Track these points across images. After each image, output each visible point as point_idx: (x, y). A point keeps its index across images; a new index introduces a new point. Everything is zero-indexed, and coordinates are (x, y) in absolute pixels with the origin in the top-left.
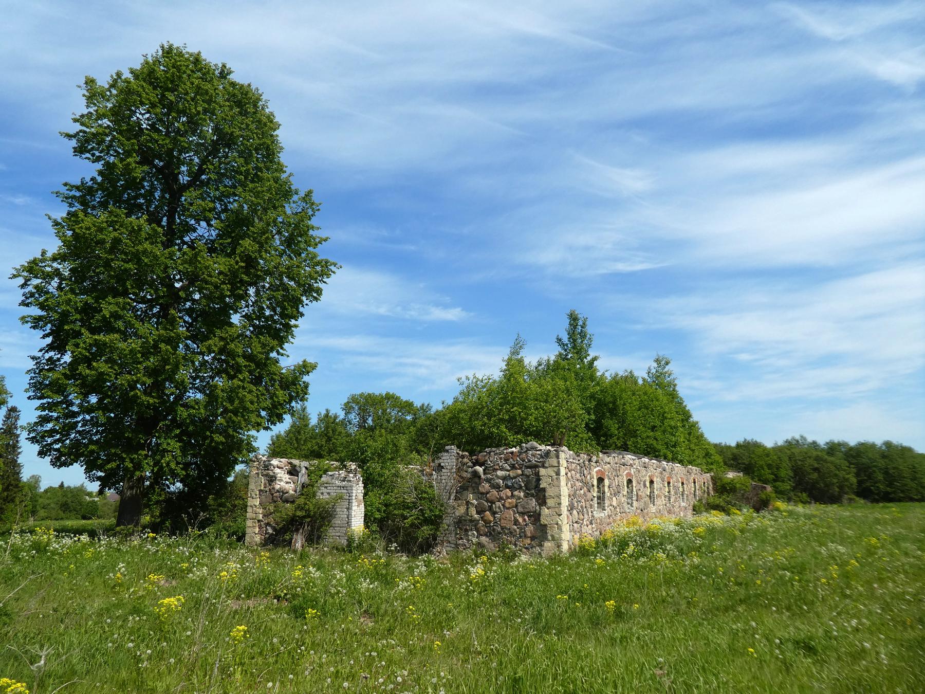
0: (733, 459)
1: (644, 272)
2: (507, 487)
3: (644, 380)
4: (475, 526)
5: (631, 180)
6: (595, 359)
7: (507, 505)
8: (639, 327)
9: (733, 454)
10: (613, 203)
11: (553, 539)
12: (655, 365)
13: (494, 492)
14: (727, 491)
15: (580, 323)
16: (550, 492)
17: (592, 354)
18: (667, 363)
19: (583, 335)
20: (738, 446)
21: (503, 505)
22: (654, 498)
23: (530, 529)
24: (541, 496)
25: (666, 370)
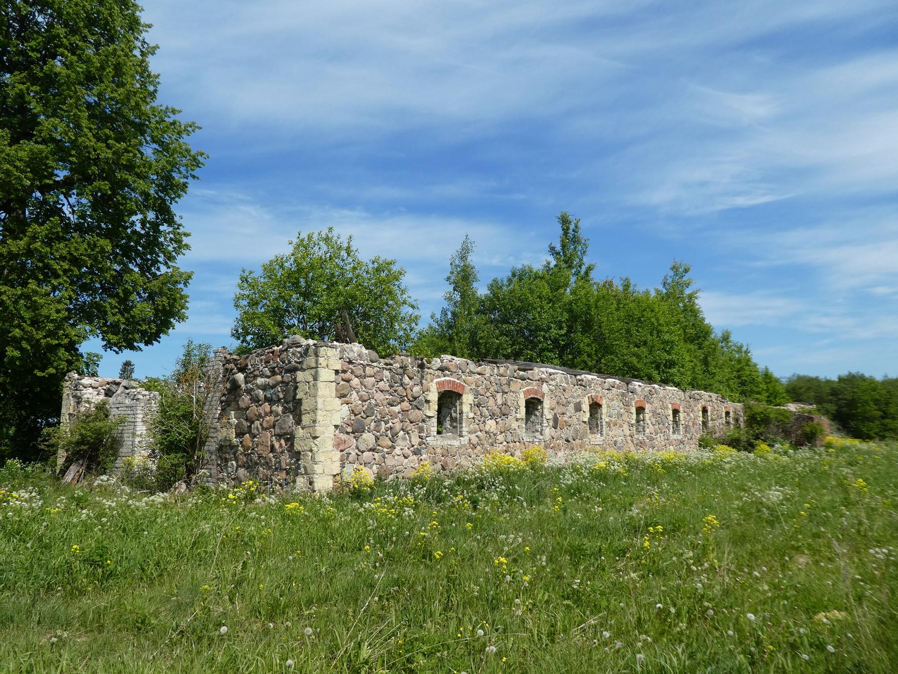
0: (832, 395)
1: (766, 205)
2: (267, 399)
3: (657, 291)
4: (234, 454)
5: (752, 106)
6: (589, 269)
7: (265, 425)
8: (758, 264)
9: (832, 389)
10: (731, 133)
11: (306, 473)
12: (672, 273)
13: (254, 407)
14: (758, 423)
15: (572, 227)
16: (305, 406)
17: (587, 261)
18: (686, 271)
19: (575, 240)
20: (841, 379)
21: (261, 425)
22: (641, 427)
23: (286, 459)
24: (295, 408)
25: (684, 279)
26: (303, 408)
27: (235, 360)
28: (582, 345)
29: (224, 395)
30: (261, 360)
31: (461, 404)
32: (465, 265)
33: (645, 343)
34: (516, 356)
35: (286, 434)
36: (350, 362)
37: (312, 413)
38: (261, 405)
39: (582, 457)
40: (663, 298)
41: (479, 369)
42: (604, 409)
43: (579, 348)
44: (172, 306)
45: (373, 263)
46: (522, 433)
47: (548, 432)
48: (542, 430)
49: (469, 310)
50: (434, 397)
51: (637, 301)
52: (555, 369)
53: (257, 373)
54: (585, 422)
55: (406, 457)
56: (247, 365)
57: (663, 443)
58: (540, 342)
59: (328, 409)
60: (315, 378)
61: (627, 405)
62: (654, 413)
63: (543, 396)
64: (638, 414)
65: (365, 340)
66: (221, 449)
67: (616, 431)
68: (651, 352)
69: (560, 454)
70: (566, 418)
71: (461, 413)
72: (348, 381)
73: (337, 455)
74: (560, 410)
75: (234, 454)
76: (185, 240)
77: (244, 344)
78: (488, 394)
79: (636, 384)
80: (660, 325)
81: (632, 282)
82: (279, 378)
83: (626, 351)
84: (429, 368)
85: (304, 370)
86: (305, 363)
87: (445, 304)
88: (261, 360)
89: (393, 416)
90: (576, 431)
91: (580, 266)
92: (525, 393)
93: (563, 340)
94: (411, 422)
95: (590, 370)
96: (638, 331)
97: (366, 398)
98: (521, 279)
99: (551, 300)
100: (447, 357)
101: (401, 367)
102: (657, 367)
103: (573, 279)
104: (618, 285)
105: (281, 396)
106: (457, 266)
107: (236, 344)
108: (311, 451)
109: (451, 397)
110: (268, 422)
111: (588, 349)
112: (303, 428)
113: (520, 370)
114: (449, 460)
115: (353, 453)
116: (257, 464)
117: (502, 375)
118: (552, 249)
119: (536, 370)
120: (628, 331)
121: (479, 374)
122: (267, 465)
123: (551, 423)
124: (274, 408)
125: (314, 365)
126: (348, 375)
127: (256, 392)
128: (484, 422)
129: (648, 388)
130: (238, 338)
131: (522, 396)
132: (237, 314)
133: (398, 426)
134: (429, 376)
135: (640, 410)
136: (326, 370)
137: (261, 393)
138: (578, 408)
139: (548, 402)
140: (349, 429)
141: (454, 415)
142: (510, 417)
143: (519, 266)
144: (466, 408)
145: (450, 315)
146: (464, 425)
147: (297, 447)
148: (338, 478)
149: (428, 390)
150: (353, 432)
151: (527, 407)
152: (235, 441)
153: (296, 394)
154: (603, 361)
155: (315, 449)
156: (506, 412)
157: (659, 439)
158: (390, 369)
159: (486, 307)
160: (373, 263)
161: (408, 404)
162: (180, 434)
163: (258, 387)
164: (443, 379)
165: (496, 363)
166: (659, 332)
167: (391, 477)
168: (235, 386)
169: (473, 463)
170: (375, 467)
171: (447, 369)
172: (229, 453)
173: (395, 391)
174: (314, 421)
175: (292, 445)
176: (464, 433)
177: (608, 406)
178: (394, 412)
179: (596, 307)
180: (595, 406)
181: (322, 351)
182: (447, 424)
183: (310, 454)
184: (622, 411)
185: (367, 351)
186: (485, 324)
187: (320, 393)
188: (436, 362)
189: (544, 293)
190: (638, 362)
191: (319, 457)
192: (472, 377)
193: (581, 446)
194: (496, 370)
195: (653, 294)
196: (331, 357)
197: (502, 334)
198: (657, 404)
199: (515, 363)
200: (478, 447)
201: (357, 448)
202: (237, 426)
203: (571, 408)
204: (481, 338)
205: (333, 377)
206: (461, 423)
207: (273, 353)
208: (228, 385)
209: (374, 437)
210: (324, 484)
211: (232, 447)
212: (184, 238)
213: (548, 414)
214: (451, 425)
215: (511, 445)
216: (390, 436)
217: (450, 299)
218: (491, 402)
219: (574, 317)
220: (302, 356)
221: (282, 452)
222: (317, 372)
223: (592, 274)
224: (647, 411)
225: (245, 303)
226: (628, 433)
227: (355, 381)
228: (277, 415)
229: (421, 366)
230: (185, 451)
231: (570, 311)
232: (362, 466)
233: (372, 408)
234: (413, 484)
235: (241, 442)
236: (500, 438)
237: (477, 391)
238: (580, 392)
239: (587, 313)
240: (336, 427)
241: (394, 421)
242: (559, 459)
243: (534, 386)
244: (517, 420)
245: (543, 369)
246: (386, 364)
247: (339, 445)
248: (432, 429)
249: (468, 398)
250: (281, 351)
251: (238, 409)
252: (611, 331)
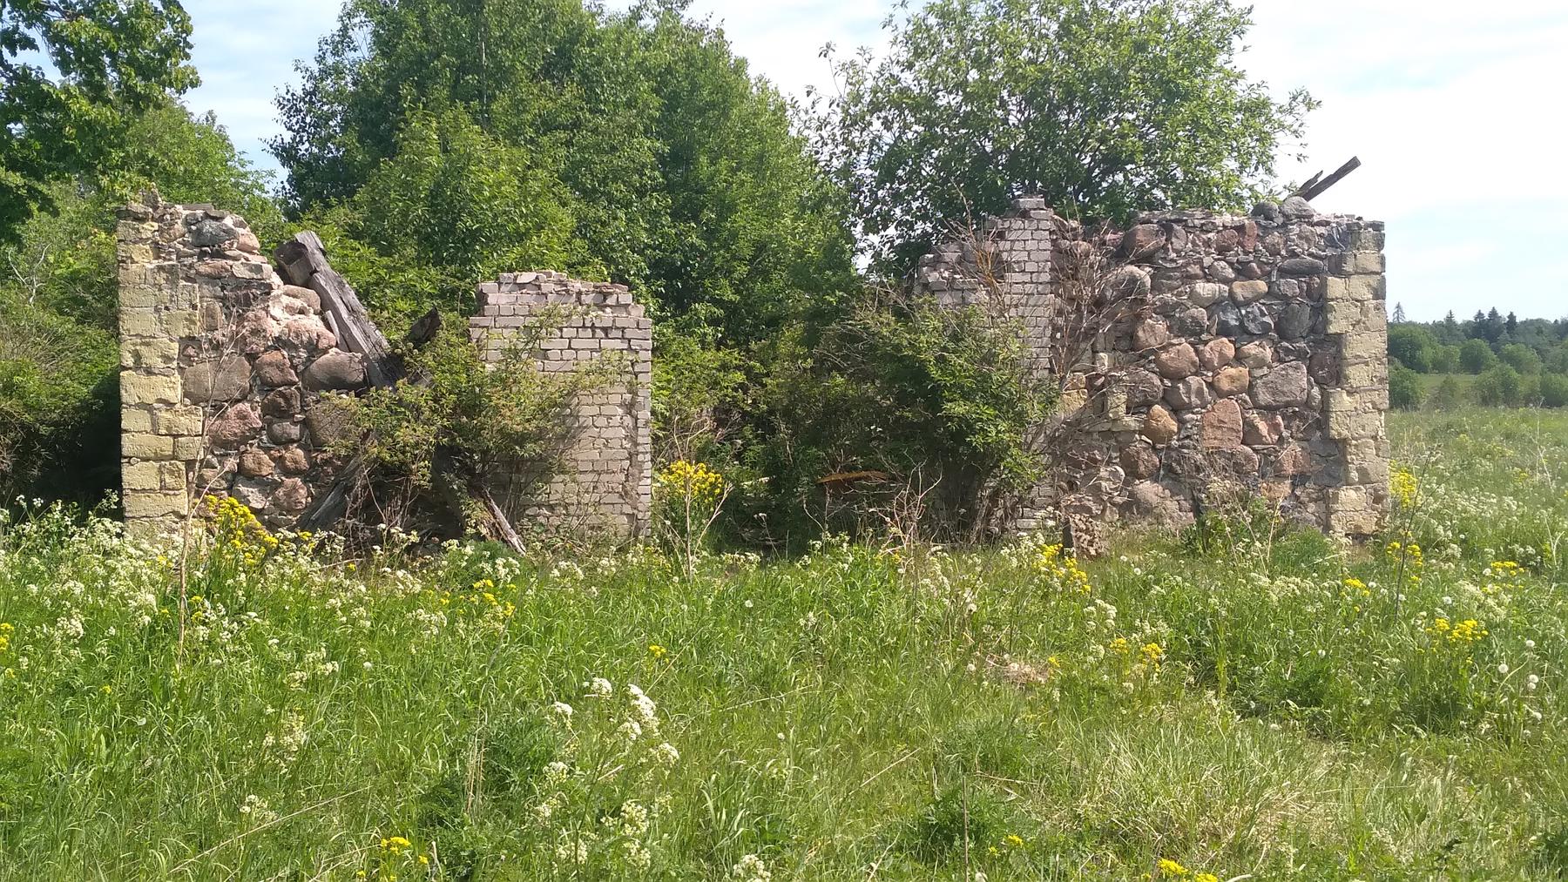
21: (1210, 385)
30: (1207, 243)
35: (1288, 405)
66: (344, 438)
110: (1232, 379)
112: (1349, 393)
125: (1377, 268)
222: (1383, 281)
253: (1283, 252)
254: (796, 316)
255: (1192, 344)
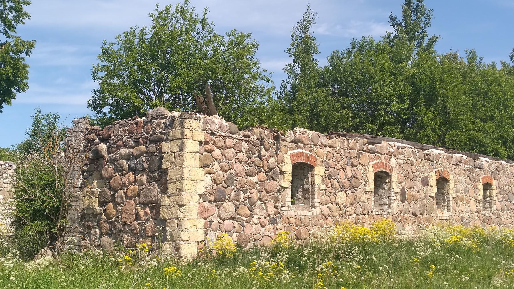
2: (130, 169)
3: (504, 64)
4: (98, 222)
11: (173, 240)
13: (117, 176)
16: (171, 175)
17: (431, 32)
19: (419, 11)
21: (125, 193)
23: (150, 226)
24: (160, 177)
26: (168, 177)
27: (97, 130)
28: (425, 119)
29: (86, 165)
30: (125, 131)
31: (313, 175)
32: (306, 37)
33: (492, 118)
34: (357, 129)
35: (151, 202)
36: (212, 134)
37: (178, 183)
38: (125, 175)
39: (431, 231)
40: (510, 72)
41: (330, 142)
42: (451, 185)
43: (422, 122)
44: (15, 75)
45: (229, 36)
46: (371, 206)
47: (396, 205)
48: (390, 204)
49: (309, 83)
50: (288, 168)
51: (483, 74)
52: (402, 143)
53: (120, 143)
54: (432, 197)
55: (263, 226)
56: (110, 136)
57: (510, 220)
58: (381, 116)
59: (193, 179)
60: (181, 148)
61: (474, 181)
62: (501, 189)
63: (391, 170)
64: (485, 190)
65: (224, 113)
66: (83, 217)
67: (462, 207)
68: (498, 127)
69: (408, 228)
70: (413, 192)
71: (313, 185)
72: (210, 152)
73: (201, 223)
74: (407, 184)
75: (98, 222)
76: (25, 9)
77: (101, 115)
78: (338, 167)
79: (483, 160)
80: (507, 100)
81: (478, 54)
82: (143, 148)
83: (471, 125)
84: (283, 140)
85: (170, 141)
86: (171, 134)
87: (286, 77)
88: (125, 131)
89: (251, 186)
90: (423, 205)
91: (423, 38)
92: (373, 166)
93: (405, 114)
94: (267, 193)
95: (434, 144)
96: (484, 105)
97: (227, 169)
98: (361, 51)
99: (392, 73)
100: (299, 130)
101: (258, 139)
102: (505, 143)
103: (415, 51)
104: (463, 58)
105: (146, 166)
106: (297, 38)
107: (92, 114)
108: (177, 218)
109: (302, 169)
110: (132, 191)
111: (432, 123)
112: (169, 197)
113: (369, 143)
114: (303, 230)
115: (216, 221)
116: (120, 231)
117: (352, 149)
118: (392, 20)
119: (384, 143)
120: (474, 106)
121: (330, 147)
122: (132, 232)
123: (399, 197)
124: (139, 177)
125: (180, 136)
126: (210, 146)
127: (120, 162)
128: (335, 194)
129: (495, 164)
130: (95, 109)
131: (371, 169)
132: (96, 85)
133: (255, 196)
134: (283, 148)
135: (487, 186)
136: (191, 141)
137: (125, 163)
138: (425, 182)
139: (396, 176)
140: (212, 198)
141: (306, 186)
142: (359, 190)
143: (359, 38)
144: (318, 180)
145: (289, 88)
146: (316, 196)
147: (163, 215)
148: (202, 245)
149: (283, 162)
150: (215, 201)
151: (375, 180)
152: (98, 209)
153: (161, 164)
154: (447, 136)
155: (181, 216)
156: (356, 185)
157: (505, 216)
158: (248, 141)
159: (324, 80)
160: (229, 36)
161: (264, 175)
162: (44, 202)
163: (122, 157)
164: (296, 151)
165: (344, 136)
166: (506, 106)
167: (250, 245)
168: (98, 156)
169: (327, 233)
170: (234, 235)
171: (300, 141)
172: (92, 221)
173: (253, 162)
174: (181, 190)
175: (158, 213)
176: (316, 204)
177: (455, 182)
178: (252, 183)
179: (441, 81)
180: (442, 181)
181: (188, 122)
182: (299, 195)
183: (176, 221)
184: (469, 186)
185: (227, 123)
186: (326, 97)
187: (186, 163)
188: (290, 135)
189: (386, 66)
190: (485, 137)
191: (186, 225)
192: (325, 150)
193: (429, 221)
194: (346, 143)
195: (499, 67)
196: (196, 128)
197: (343, 107)
198: (504, 180)
199: (363, 137)
200: (330, 218)
201: (219, 216)
202: (100, 195)
203: (419, 182)
204: (321, 111)
205: (197, 148)
206: (313, 195)
207: (136, 124)
208: (91, 156)
209: (233, 206)
210: (189, 250)
211: (95, 215)
212: (24, 7)
213: (396, 188)
214: (303, 196)
215: (361, 217)
216: (248, 205)
217: (290, 71)
218: (341, 174)
219: (417, 91)
220: (167, 127)
221: (147, 220)
222: (182, 143)
223: (436, 47)
224: (494, 187)
225: (102, 74)
226: (474, 208)
227: (217, 152)
228: (142, 184)
229: (277, 139)
230: (48, 218)
231: (413, 84)
232: (224, 234)
233: (232, 178)
234: (274, 253)
235: (104, 211)
236: (349, 209)
237: (328, 164)
238: (427, 166)
239: (432, 86)
240: (200, 195)
241: (252, 191)
242: (408, 232)
243: (383, 159)
244: (366, 193)
245: (392, 143)
246: (245, 136)
247: (203, 213)
248: (287, 199)
249: (320, 171)
250: (145, 123)
251: (101, 178)
252: (456, 105)
253: (151, 133)
254: (135, 177)
255: (120, 176)
